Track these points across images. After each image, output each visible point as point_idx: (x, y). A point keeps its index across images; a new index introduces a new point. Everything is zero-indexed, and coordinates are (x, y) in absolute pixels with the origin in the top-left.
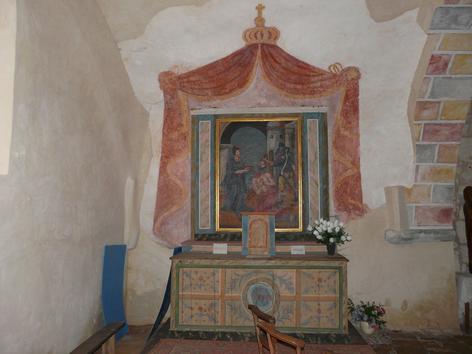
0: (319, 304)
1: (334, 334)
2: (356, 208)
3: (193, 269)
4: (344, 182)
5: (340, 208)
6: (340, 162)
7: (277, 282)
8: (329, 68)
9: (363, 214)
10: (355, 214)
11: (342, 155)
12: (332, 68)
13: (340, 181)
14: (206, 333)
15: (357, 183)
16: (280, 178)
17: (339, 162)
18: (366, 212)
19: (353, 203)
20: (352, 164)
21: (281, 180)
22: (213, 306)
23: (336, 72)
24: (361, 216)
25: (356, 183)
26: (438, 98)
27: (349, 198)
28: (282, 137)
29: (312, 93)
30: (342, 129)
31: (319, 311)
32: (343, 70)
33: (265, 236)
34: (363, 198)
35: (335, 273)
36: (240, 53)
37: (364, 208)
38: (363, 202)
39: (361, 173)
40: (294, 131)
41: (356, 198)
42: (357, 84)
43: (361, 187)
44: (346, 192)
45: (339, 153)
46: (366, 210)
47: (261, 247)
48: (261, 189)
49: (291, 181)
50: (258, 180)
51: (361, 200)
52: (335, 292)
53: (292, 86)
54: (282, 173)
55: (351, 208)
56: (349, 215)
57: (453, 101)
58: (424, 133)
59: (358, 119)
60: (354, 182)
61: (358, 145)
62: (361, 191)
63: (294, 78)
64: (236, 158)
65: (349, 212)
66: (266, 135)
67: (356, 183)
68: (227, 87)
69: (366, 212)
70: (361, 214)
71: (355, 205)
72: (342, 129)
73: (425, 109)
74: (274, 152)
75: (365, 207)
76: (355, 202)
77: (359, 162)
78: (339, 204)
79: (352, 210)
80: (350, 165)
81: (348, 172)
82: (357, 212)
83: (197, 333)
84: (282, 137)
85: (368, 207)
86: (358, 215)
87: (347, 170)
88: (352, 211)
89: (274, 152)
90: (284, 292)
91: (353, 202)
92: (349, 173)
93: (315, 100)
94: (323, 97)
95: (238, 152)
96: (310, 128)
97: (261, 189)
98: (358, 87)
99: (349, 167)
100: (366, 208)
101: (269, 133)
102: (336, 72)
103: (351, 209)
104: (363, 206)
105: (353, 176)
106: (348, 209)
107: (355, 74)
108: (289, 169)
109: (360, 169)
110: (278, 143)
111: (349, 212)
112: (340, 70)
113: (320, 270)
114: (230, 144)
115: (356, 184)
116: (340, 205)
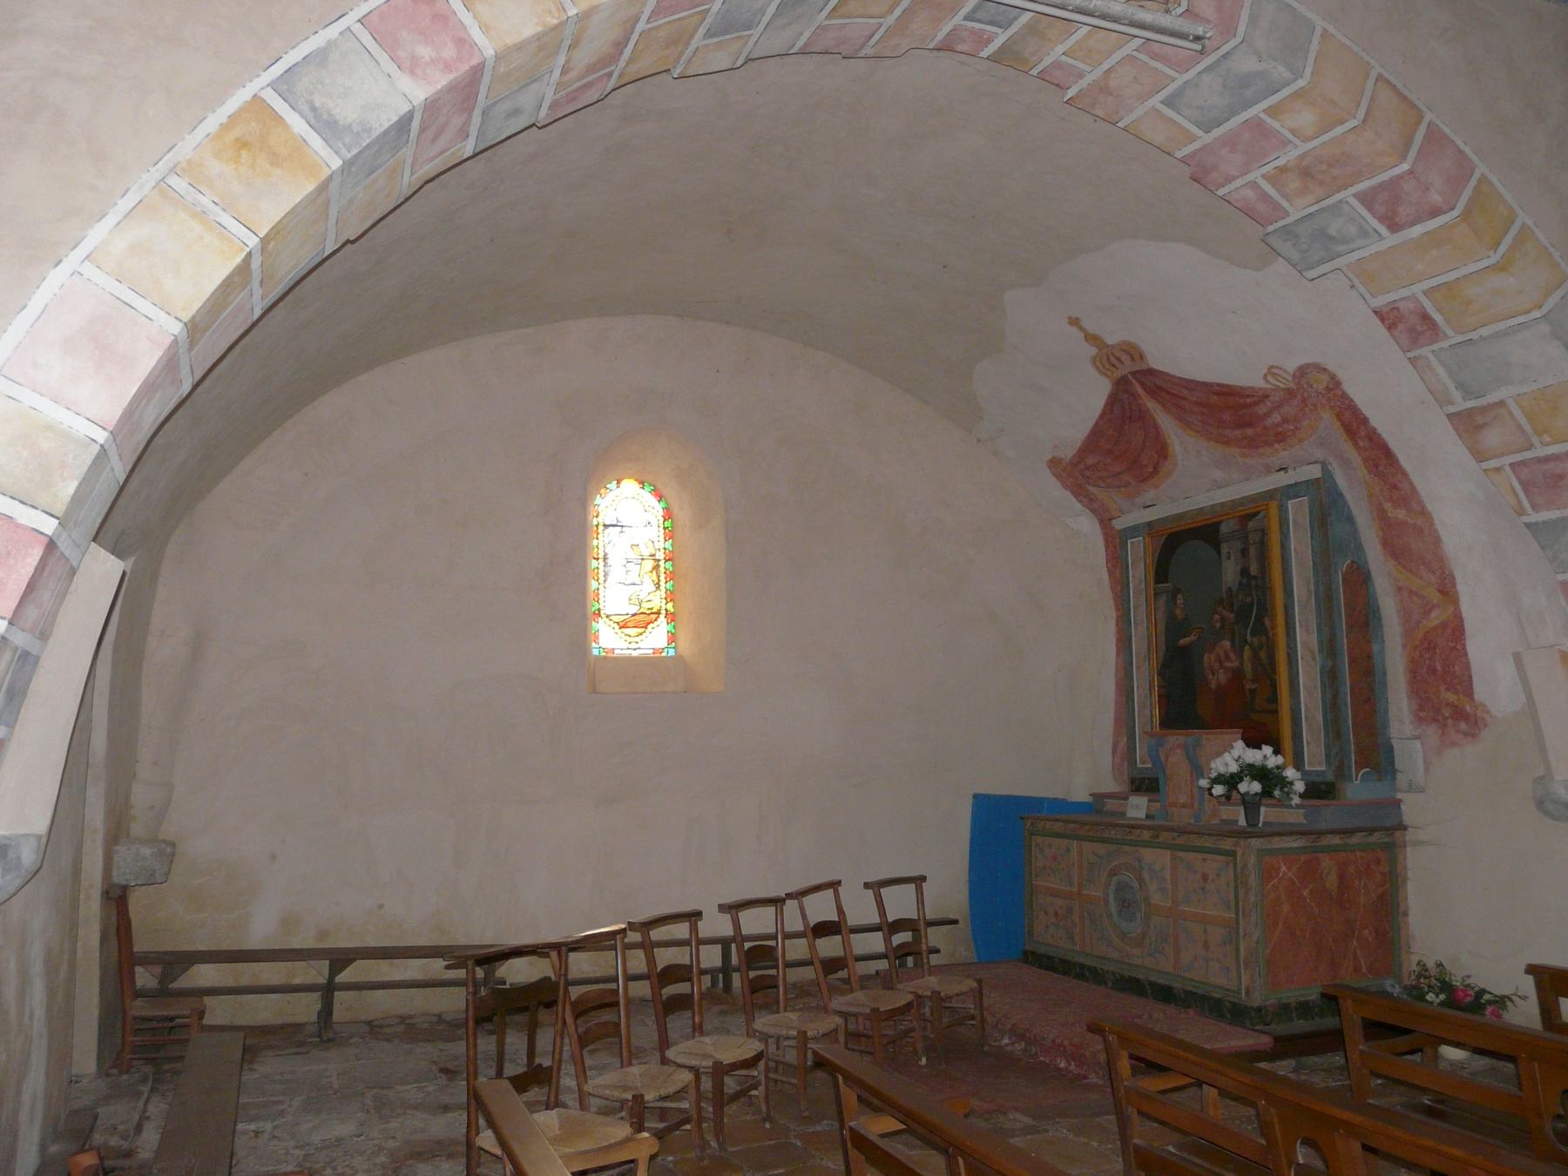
0: (1205, 931)
1: (1230, 1002)
2: (1460, 714)
3: (1048, 840)
4: (1426, 645)
5: (1422, 714)
6: (1411, 590)
7: (1146, 875)
8: (1265, 377)
9: (1477, 731)
10: (1458, 731)
11: (1411, 571)
12: (1270, 378)
13: (1417, 642)
14: (1063, 961)
15: (1456, 643)
16: (1247, 647)
17: (1411, 592)
18: (1486, 725)
19: (1452, 700)
20: (1441, 592)
21: (1247, 653)
22: (1069, 910)
23: (1285, 384)
24: (1474, 736)
25: (1454, 644)
26: (1489, 396)
27: (1443, 688)
28: (1244, 552)
29: (1280, 437)
30: (1388, 506)
31: (1206, 946)
32: (1294, 376)
33: (1189, 782)
34: (1474, 686)
35: (1228, 864)
36: (1112, 401)
37: (1479, 713)
38: (1476, 696)
39: (1464, 615)
40: (1264, 535)
41: (1458, 687)
42: (1344, 396)
43: (1466, 654)
44: (1434, 671)
45: (1404, 567)
46: (1483, 719)
47: (1184, 806)
48: (1218, 679)
49: (1263, 654)
50: (1213, 657)
51: (1469, 693)
52: (1229, 908)
53: (1237, 432)
54: (1249, 637)
55: (1447, 714)
56: (1443, 734)
57: (1533, 391)
58: (1526, 491)
59: (1405, 474)
60: (1450, 644)
61: (1437, 541)
62: (1467, 666)
63: (1227, 416)
64: (1178, 612)
65: (1444, 726)
66: (1219, 553)
67: (1454, 644)
68: (1145, 462)
69: (1486, 725)
70: (1473, 731)
71: (1457, 706)
72: (1388, 506)
73: (1479, 428)
74: (1234, 590)
75: (1480, 710)
76: (1455, 697)
77: (1454, 585)
78: (1420, 705)
79: (1450, 720)
80: (1436, 597)
81: (1434, 614)
82: (1463, 726)
83: (1051, 958)
84: (1244, 552)
85: (1488, 712)
86: (1466, 734)
87: (1430, 611)
88: (1450, 722)
89: (1234, 590)
90: (1156, 898)
91: (1450, 697)
92: (1436, 618)
93: (1282, 455)
94: (1306, 442)
95: (1180, 600)
96: (1295, 522)
97: (1218, 679)
98: (1352, 401)
99: (1435, 602)
100: (1485, 715)
101: (1225, 549)
102: (1285, 384)
103: (1447, 718)
104: (1477, 709)
105: (1444, 625)
106: (1440, 718)
107: (1325, 378)
108: (1260, 629)
109: (1459, 606)
110: (1239, 568)
111: (1444, 726)
112: (1290, 378)
113: (1206, 856)
114: (1168, 582)
115: (1455, 647)
116: (1421, 708)
